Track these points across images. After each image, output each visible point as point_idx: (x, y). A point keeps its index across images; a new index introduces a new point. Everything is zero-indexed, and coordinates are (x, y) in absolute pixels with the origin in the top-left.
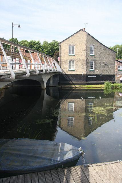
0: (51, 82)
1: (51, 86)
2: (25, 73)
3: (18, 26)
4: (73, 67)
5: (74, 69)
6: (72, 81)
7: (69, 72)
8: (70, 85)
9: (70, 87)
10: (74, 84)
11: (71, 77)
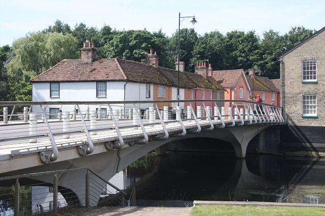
0: (261, 144)
1: (261, 154)
2: (210, 126)
3: (192, 19)
4: (313, 109)
5: (315, 115)
6: (310, 143)
7: (304, 120)
8: (307, 151)
9: (306, 157)
10: (315, 149)
11: (308, 135)
